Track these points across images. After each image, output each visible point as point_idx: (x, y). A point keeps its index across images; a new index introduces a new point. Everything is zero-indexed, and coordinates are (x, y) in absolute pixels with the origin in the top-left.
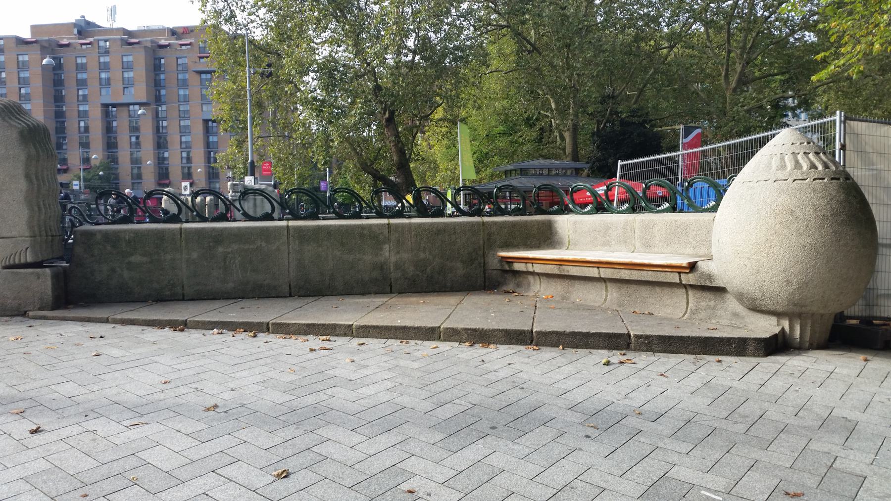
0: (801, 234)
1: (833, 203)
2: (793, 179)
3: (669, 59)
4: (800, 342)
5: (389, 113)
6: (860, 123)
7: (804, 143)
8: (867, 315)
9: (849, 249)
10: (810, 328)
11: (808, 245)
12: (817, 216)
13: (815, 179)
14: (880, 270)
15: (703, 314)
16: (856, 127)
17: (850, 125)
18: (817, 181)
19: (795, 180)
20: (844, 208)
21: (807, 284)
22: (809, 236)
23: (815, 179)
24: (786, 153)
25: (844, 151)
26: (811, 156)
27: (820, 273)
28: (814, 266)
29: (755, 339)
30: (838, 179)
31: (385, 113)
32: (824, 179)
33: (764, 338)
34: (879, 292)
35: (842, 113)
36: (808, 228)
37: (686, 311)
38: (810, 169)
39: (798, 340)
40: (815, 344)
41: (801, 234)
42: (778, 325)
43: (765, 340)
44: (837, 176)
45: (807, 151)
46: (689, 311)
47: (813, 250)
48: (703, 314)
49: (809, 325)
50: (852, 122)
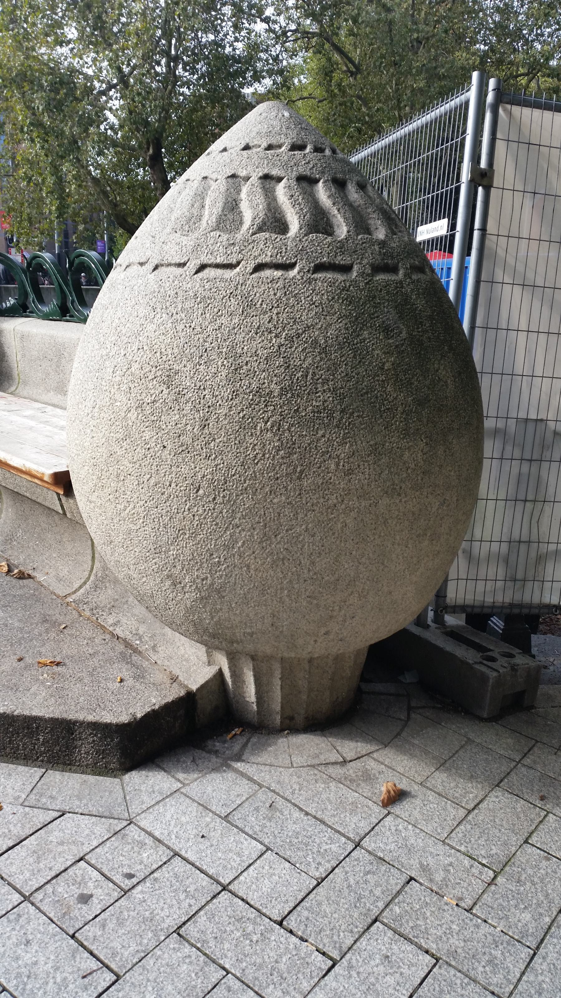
0: (185, 449)
1: (297, 351)
2: (198, 262)
3: (476, 64)
4: (259, 712)
5: (153, 149)
6: (537, 113)
7: (280, 146)
8: (507, 600)
9: (333, 500)
10: (279, 683)
11: (204, 484)
12: (235, 394)
13: (259, 268)
14: (550, 496)
15: (109, 591)
16: (536, 127)
17: (510, 114)
18: (268, 273)
19: (202, 267)
20: (333, 368)
21: (218, 591)
22: (208, 457)
23: (259, 268)
24: (214, 176)
25: (488, 189)
26: (281, 191)
27: (248, 566)
28: (226, 547)
29: (95, 726)
30: (346, 269)
31: (148, 149)
32: (292, 266)
33: (117, 725)
34: (543, 548)
35: (492, 83)
36: (206, 431)
37: (88, 578)
38: (260, 229)
39: (255, 707)
40: (300, 720)
41: (185, 449)
42: (209, 664)
43: (121, 728)
44: (339, 260)
45: (275, 172)
46: (92, 578)
47: (219, 500)
48: (109, 591)
49: (278, 674)
50: (516, 110)
